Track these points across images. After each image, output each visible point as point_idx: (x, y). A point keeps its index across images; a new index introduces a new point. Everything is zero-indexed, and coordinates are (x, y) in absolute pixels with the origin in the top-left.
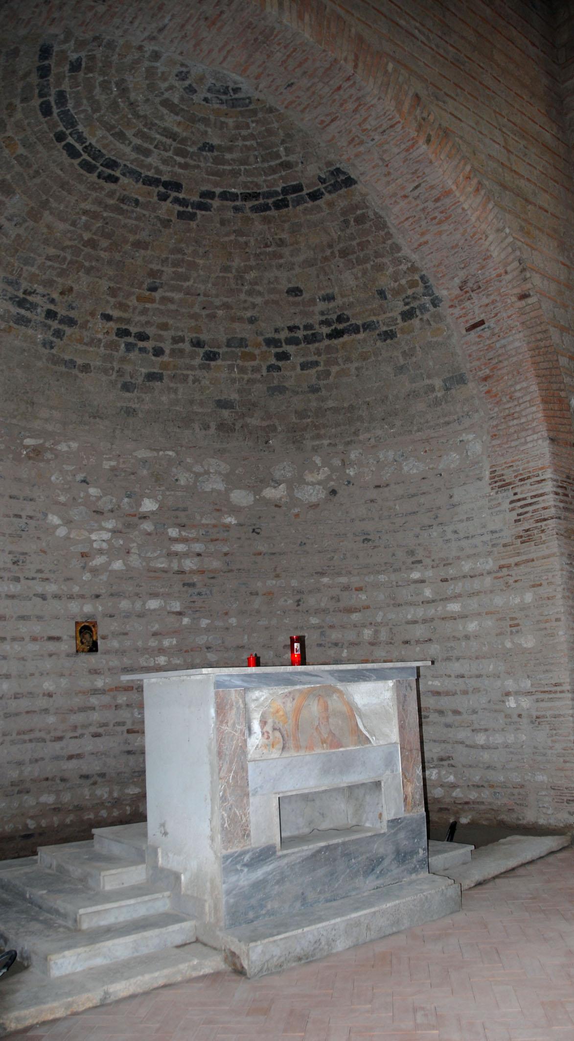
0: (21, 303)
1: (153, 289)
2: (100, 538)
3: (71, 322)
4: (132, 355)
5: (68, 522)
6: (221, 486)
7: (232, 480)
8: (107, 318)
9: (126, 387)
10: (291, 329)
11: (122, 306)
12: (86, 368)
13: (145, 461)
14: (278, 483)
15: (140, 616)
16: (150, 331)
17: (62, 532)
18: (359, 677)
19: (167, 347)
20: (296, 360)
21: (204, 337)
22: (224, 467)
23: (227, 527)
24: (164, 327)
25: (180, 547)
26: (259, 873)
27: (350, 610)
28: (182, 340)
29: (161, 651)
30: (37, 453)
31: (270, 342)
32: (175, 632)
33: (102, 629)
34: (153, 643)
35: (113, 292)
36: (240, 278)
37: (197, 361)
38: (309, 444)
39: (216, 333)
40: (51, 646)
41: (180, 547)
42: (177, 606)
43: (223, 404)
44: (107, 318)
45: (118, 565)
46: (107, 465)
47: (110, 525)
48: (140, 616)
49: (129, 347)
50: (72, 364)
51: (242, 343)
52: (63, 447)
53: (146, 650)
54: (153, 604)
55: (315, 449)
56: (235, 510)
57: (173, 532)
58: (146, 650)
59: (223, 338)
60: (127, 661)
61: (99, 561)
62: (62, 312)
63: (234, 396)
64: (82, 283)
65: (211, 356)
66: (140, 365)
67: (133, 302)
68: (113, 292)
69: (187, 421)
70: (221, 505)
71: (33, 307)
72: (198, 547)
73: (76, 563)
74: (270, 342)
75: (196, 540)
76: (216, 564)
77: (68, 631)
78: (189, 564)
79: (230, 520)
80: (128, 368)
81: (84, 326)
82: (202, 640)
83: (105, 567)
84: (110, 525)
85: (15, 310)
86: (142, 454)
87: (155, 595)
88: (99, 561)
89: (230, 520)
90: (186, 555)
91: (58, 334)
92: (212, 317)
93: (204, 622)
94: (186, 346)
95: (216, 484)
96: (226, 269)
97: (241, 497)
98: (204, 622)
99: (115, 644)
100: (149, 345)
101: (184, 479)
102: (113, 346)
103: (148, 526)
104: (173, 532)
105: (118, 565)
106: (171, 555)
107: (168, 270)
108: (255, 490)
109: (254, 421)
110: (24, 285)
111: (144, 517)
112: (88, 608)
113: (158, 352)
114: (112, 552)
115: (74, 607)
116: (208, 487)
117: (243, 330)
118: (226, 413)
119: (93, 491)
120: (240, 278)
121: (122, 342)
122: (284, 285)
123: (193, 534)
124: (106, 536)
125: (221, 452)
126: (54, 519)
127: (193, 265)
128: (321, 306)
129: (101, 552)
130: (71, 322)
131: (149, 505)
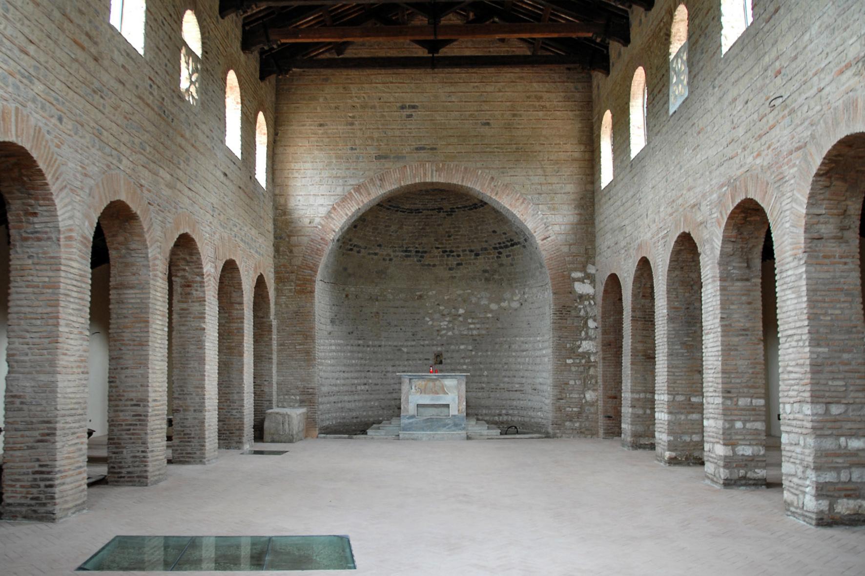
0: (406, 251)
1: (449, 236)
2: (444, 324)
3: (425, 252)
4: (450, 258)
5: (432, 320)
6: (486, 303)
7: (491, 300)
8: (438, 248)
9: (450, 269)
10: (499, 243)
11: (442, 244)
12: (434, 265)
13: (459, 295)
14: (505, 300)
15: (458, 351)
16: (454, 249)
17: (430, 323)
18: (444, 377)
19: (461, 253)
20: (504, 254)
21: (473, 248)
22: (488, 295)
23: (488, 318)
24: (458, 247)
25: (472, 326)
26: (411, 421)
27: (523, 351)
28: (465, 251)
29: (465, 364)
30: (421, 297)
31: (495, 248)
32: (470, 357)
33: (445, 355)
34: (462, 361)
35: (436, 240)
36: (476, 229)
37: (473, 257)
38: (514, 285)
39: (477, 247)
40: (426, 362)
41: (472, 326)
42: (470, 348)
43: (485, 271)
44: (438, 248)
45: (450, 333)
46: (446, 298)
47: (447, 319)
48: (458, 351)
49: (448, 256)
50: (429, 265)
51: (486, 249)
52: (430, 293)
53: (459, 363)
54: (462, 347)
55: (516, 287)
56: (491, 311)
57: (470, 321)
58: (459, 363)
59: (479, 248)
60: (453, 367)
61: (444, 332)
62: (421, 250)
63: (488, 268)
64: (425, 240)
65: (477, 255)
66: (452, 261)
67: (444, 241)
68: (436, 240)
69: (474, 278)
70: (487, 309)
71: (410, 251)
72: (478, 326)
73: (435, 333)
74: (495, 248)
75: (478, 323)
76: (484, 332)
77: (431, 357)
78: (475, 332)
79: (490, 315)
80: (449, 263)
81: (430, 252)
82: (478, 360)
83: (445, 335)
84: (447, 319)
85: (404, 254)
86: (460, 292)
87: (463, 344)
88: (444, 332)
89: (490, 315)
90: (474, 329)
91: (422, 257)
92: (473, 242)
93: (480, 354)
94: (468, 252)
95: (484, 302)
96: (471, 227)
97: (494, 306)
98: (480, 354)
99: (449, 361)
100: (455, 254)
101: (474, 300)
102: (442, 256)
103: (461, 319)
104: (470, 321)
105: (450, 333)
106: (469, 329)
107: (452, 230)
108: (498, 303)
109: (496, 277)
110: (405, 246)
111: (460, 316)
112: (439, 349)
113: (459, 256)
114: (448, 329)
115: (435, 348)
116: (482, 303)
117: (485, 245)
118: (486, 275)
119: (441, 308)
120: (476, 229)
121: (445, 254)
122: (491, 230)
123: (476, 321)
124: (446, 323)
125: (487, 289)
126: (428, 319)
127: (459, 227)
128: (504, 236)
129: (444, 329)
130: (425, 252)
131: (461, 311)
